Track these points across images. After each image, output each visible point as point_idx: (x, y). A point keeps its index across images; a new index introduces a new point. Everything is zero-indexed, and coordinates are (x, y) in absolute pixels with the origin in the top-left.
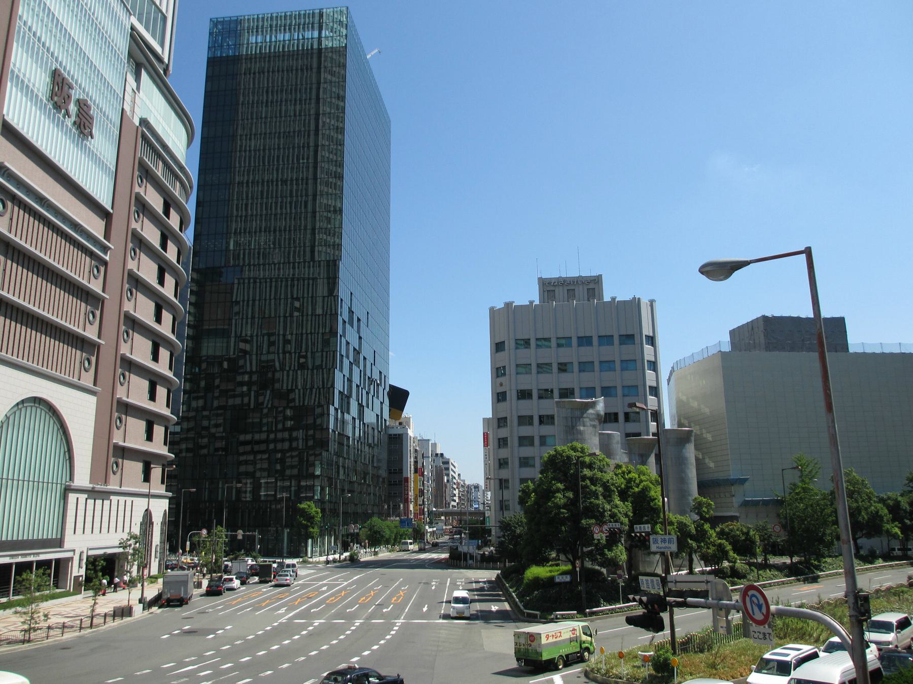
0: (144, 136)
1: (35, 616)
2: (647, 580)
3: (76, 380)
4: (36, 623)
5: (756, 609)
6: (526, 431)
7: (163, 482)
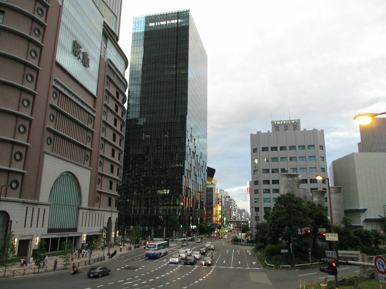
0: (109, 65)
1: (68, 259)
2: (329, 253)
3: (82, 165)
4: (69, 262)
5: (381, 267)
6: (267, 186)
7: (116, 206)
